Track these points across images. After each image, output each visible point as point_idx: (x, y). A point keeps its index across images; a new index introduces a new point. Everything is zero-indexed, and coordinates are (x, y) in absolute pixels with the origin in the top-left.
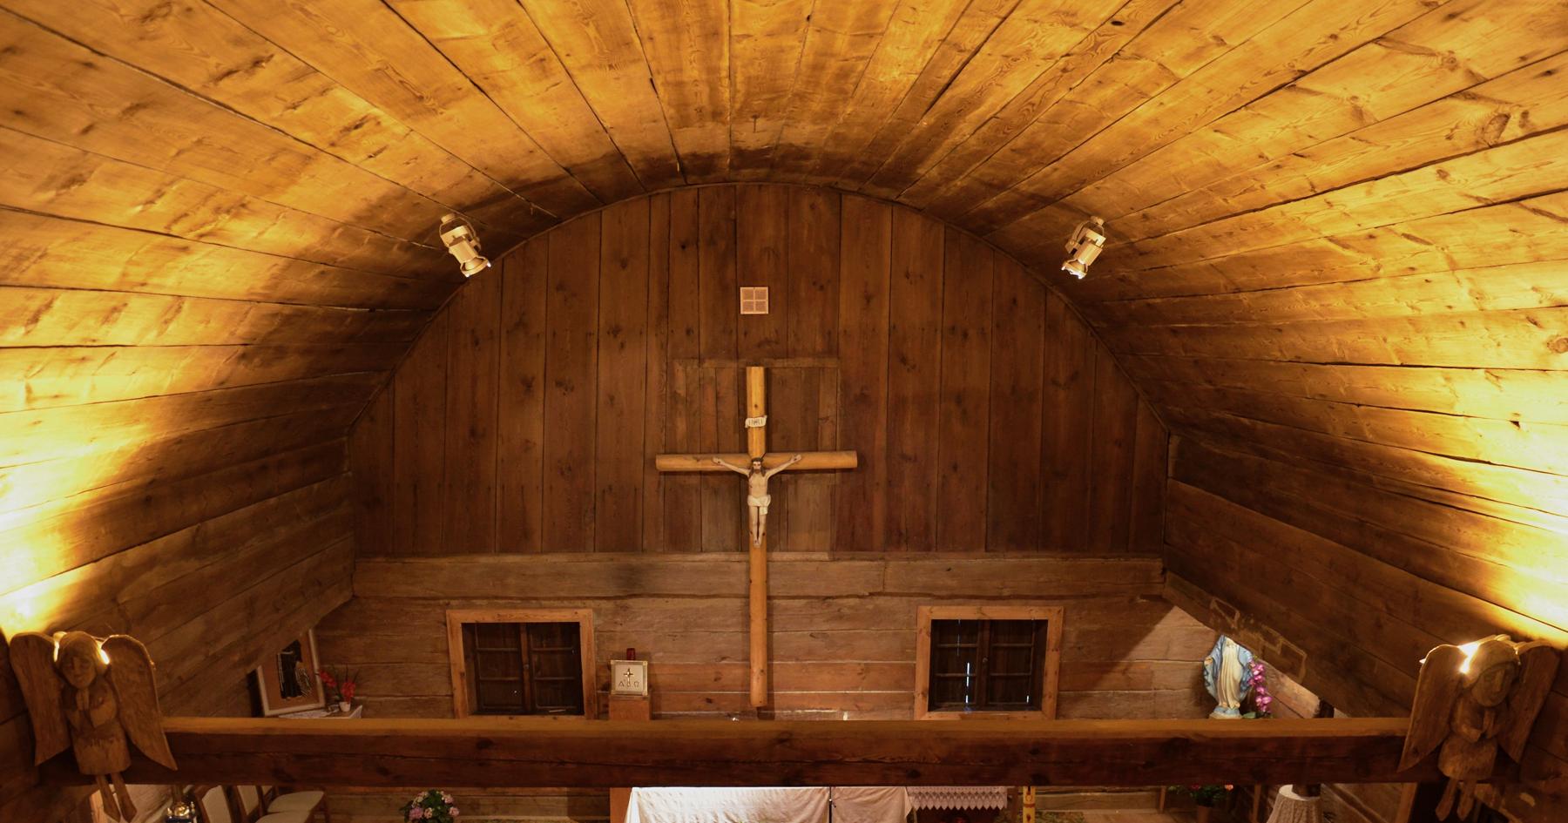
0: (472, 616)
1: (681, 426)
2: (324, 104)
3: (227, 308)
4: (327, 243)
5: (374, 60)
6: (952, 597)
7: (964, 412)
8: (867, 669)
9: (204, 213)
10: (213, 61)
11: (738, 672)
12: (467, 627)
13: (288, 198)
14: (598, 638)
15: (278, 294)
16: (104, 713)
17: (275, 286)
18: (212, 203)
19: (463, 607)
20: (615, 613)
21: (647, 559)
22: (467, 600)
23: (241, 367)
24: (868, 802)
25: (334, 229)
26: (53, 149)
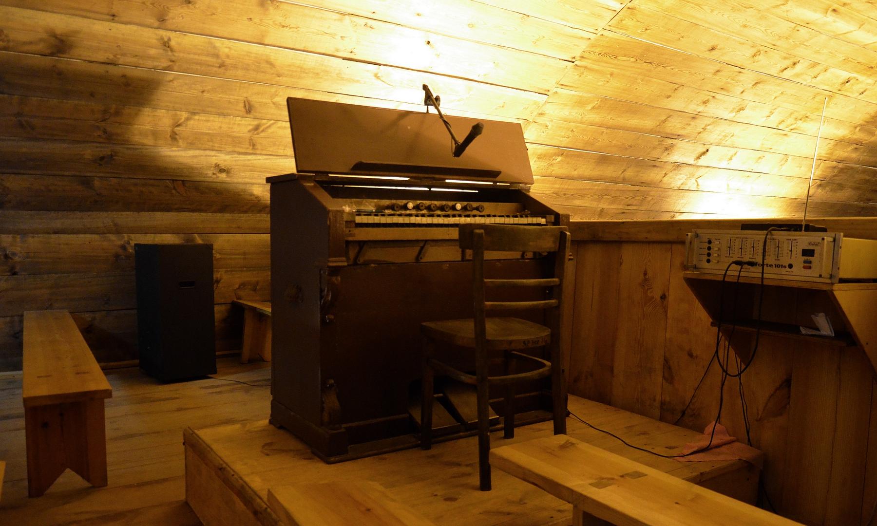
2: (828, 74)
3: (809, 162)
4: (854, 133)
5: (841, 57)
9: (790, 121)
10: (778, 65)
13: (827, 112)
15: (835, 157)
17: (832, 154)
18: (793, 116)
23: (820, 191)
25: (856, 128)
26: (734, 100)
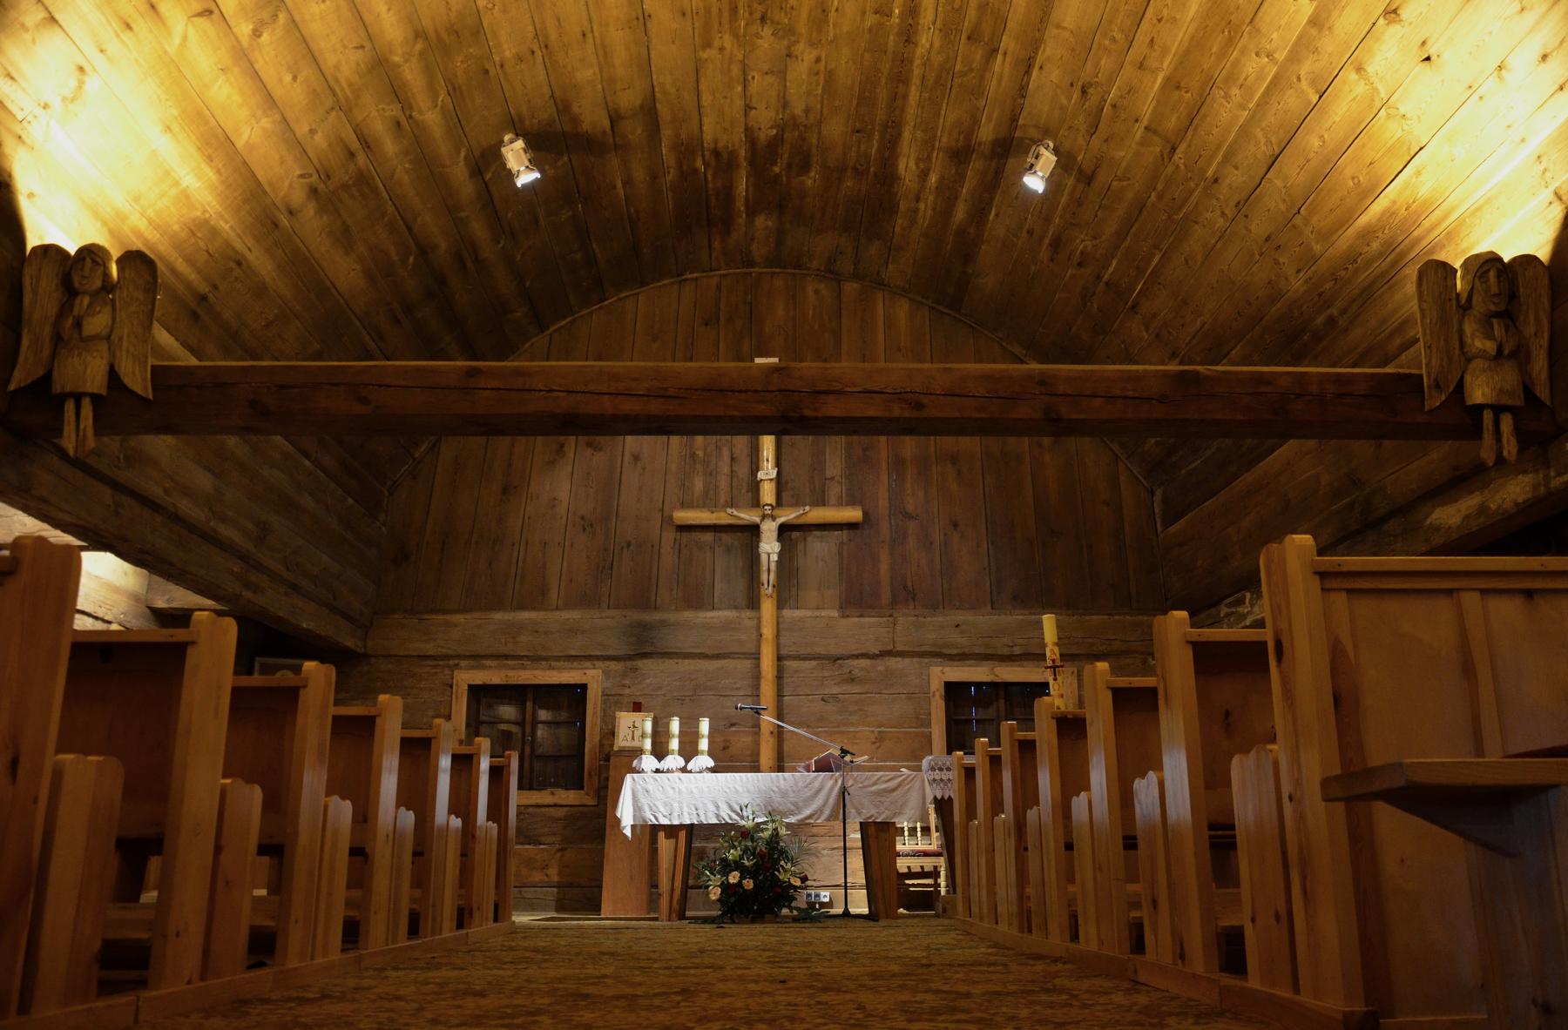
0: (480, 677)
1: (699, 484)
6: (963, 657)
7: (959, 473)
8: (880, 738)
11: (748, 739)
12: (473, 689)
14: (604, 702)
16: (97, 323)
19: (473, 668)
20: (624, 675)
21: (657, 616)
22: (477, 659)
24: (884, 790)
